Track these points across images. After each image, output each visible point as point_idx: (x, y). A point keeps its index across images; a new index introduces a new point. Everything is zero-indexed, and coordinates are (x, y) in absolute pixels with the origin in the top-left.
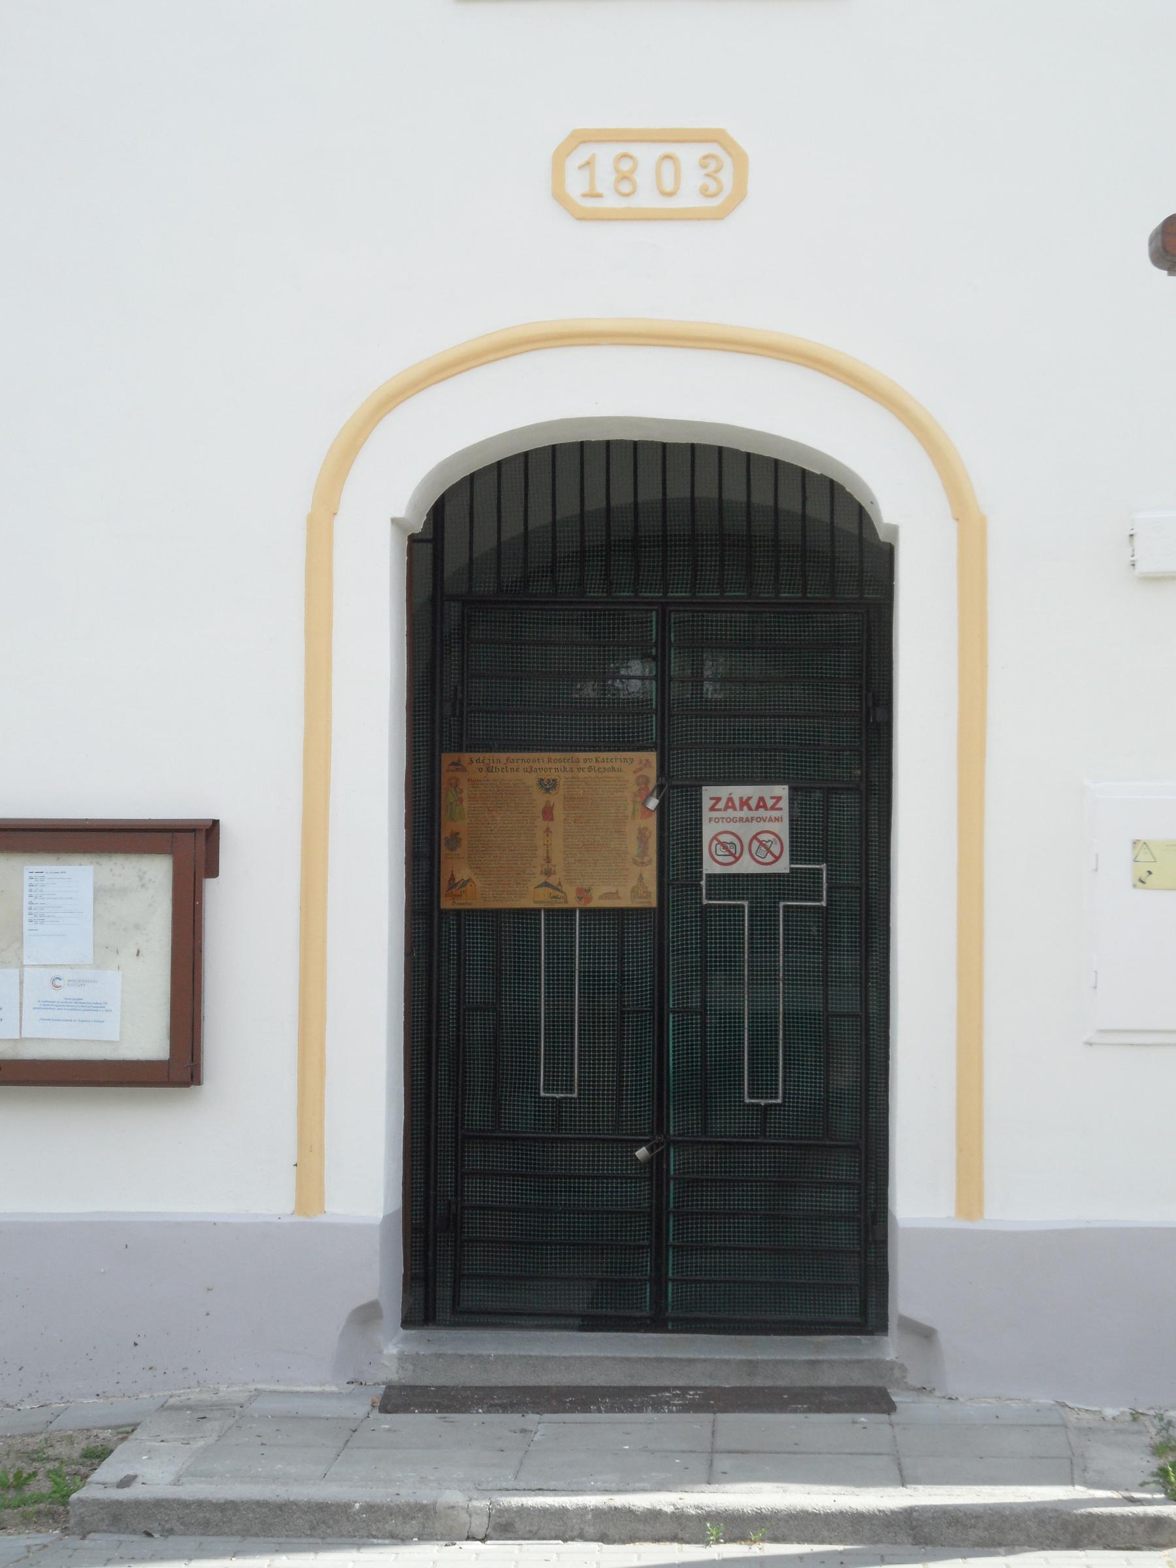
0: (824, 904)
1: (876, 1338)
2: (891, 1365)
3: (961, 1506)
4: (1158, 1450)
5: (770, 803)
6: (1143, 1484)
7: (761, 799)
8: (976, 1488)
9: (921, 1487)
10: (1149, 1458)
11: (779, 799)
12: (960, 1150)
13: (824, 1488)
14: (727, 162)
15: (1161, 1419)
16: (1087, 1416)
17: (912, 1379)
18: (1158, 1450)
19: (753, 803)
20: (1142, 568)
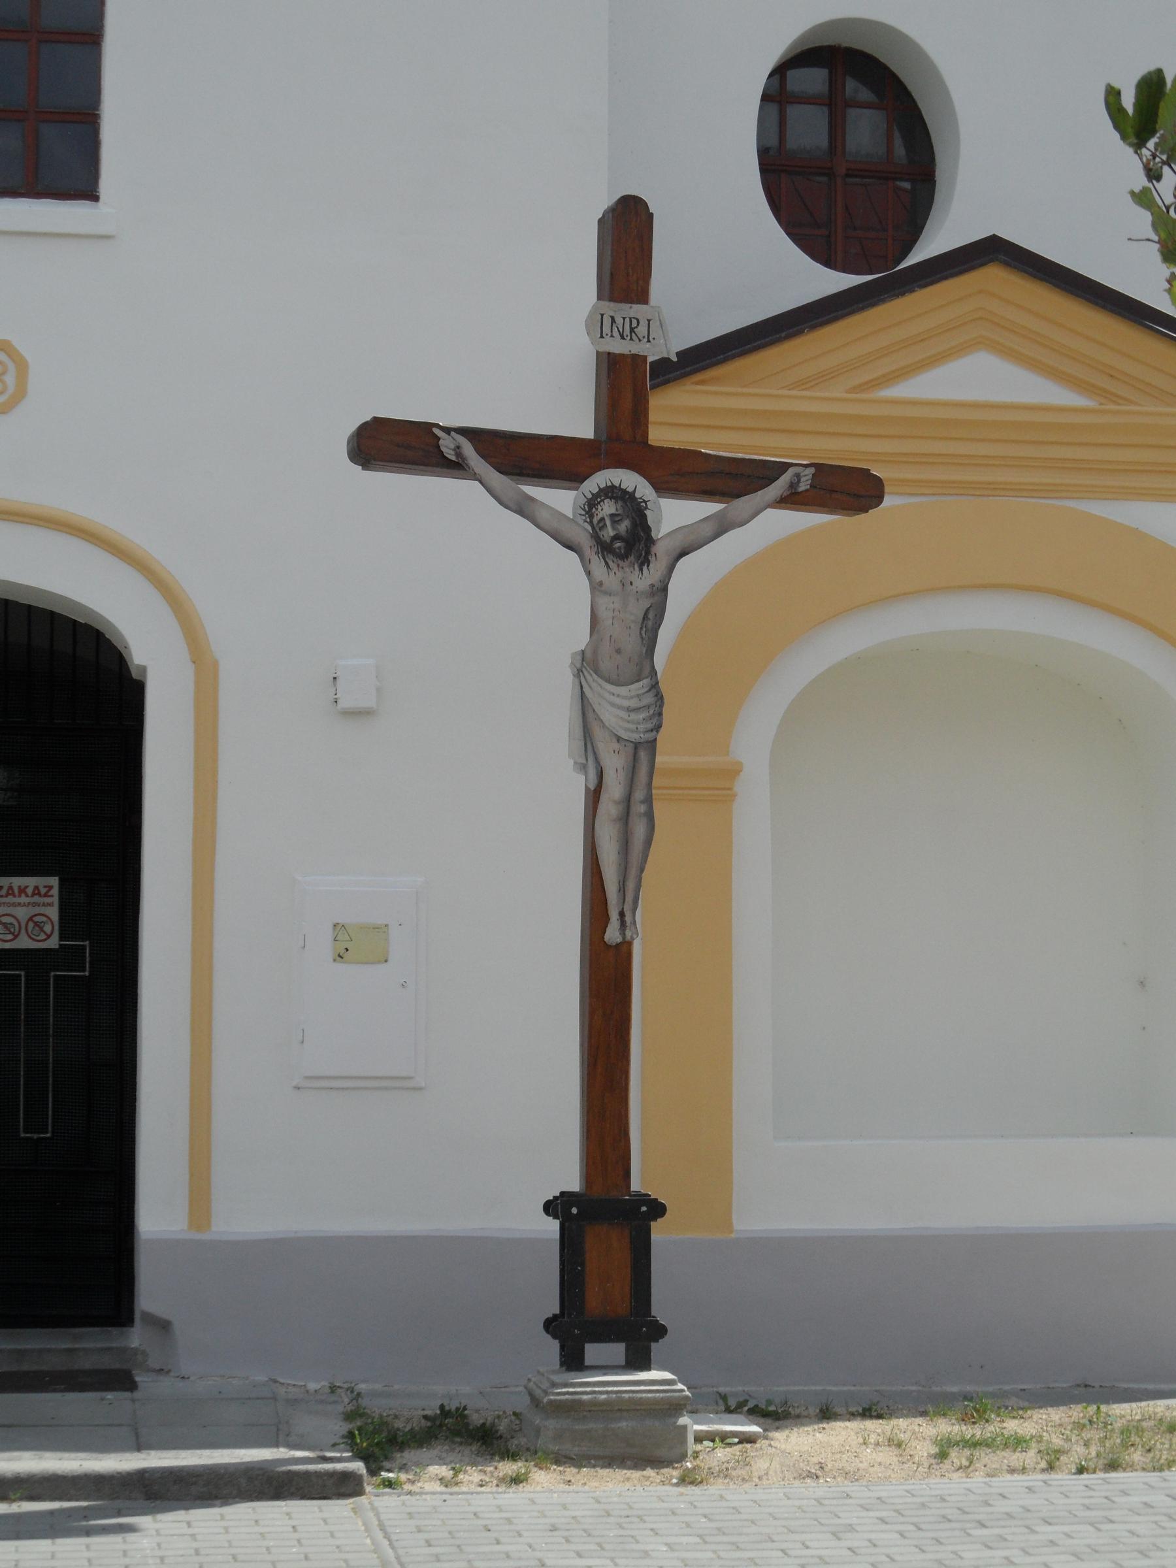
0: (87, 974)
1: (125, 1329)
2: (135, 1351)
3: (184, 1467)
4: (349, 1417)
5: (43, 891)
6: (334, 1445)
7: (36, 888)
8: (198, 1452)
9: (153, 1453)
10: (342, 1423)
11: (50, 888)
12: (192, 1175)
13: (73, 1455)
14: (11, 366)
15: (352, 1392)
16: (294, 1389)
17: (153, 1363)
18: (349, 1417)
19: (30, 891)
20: (342, 704)
